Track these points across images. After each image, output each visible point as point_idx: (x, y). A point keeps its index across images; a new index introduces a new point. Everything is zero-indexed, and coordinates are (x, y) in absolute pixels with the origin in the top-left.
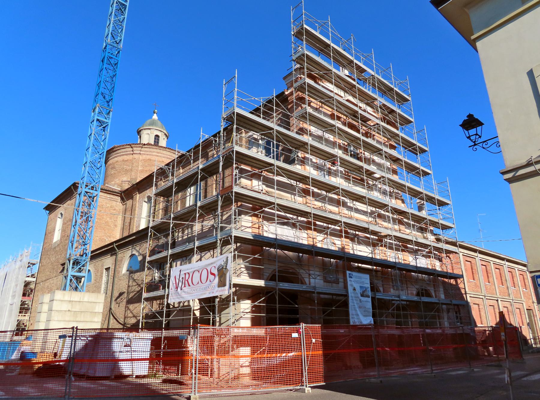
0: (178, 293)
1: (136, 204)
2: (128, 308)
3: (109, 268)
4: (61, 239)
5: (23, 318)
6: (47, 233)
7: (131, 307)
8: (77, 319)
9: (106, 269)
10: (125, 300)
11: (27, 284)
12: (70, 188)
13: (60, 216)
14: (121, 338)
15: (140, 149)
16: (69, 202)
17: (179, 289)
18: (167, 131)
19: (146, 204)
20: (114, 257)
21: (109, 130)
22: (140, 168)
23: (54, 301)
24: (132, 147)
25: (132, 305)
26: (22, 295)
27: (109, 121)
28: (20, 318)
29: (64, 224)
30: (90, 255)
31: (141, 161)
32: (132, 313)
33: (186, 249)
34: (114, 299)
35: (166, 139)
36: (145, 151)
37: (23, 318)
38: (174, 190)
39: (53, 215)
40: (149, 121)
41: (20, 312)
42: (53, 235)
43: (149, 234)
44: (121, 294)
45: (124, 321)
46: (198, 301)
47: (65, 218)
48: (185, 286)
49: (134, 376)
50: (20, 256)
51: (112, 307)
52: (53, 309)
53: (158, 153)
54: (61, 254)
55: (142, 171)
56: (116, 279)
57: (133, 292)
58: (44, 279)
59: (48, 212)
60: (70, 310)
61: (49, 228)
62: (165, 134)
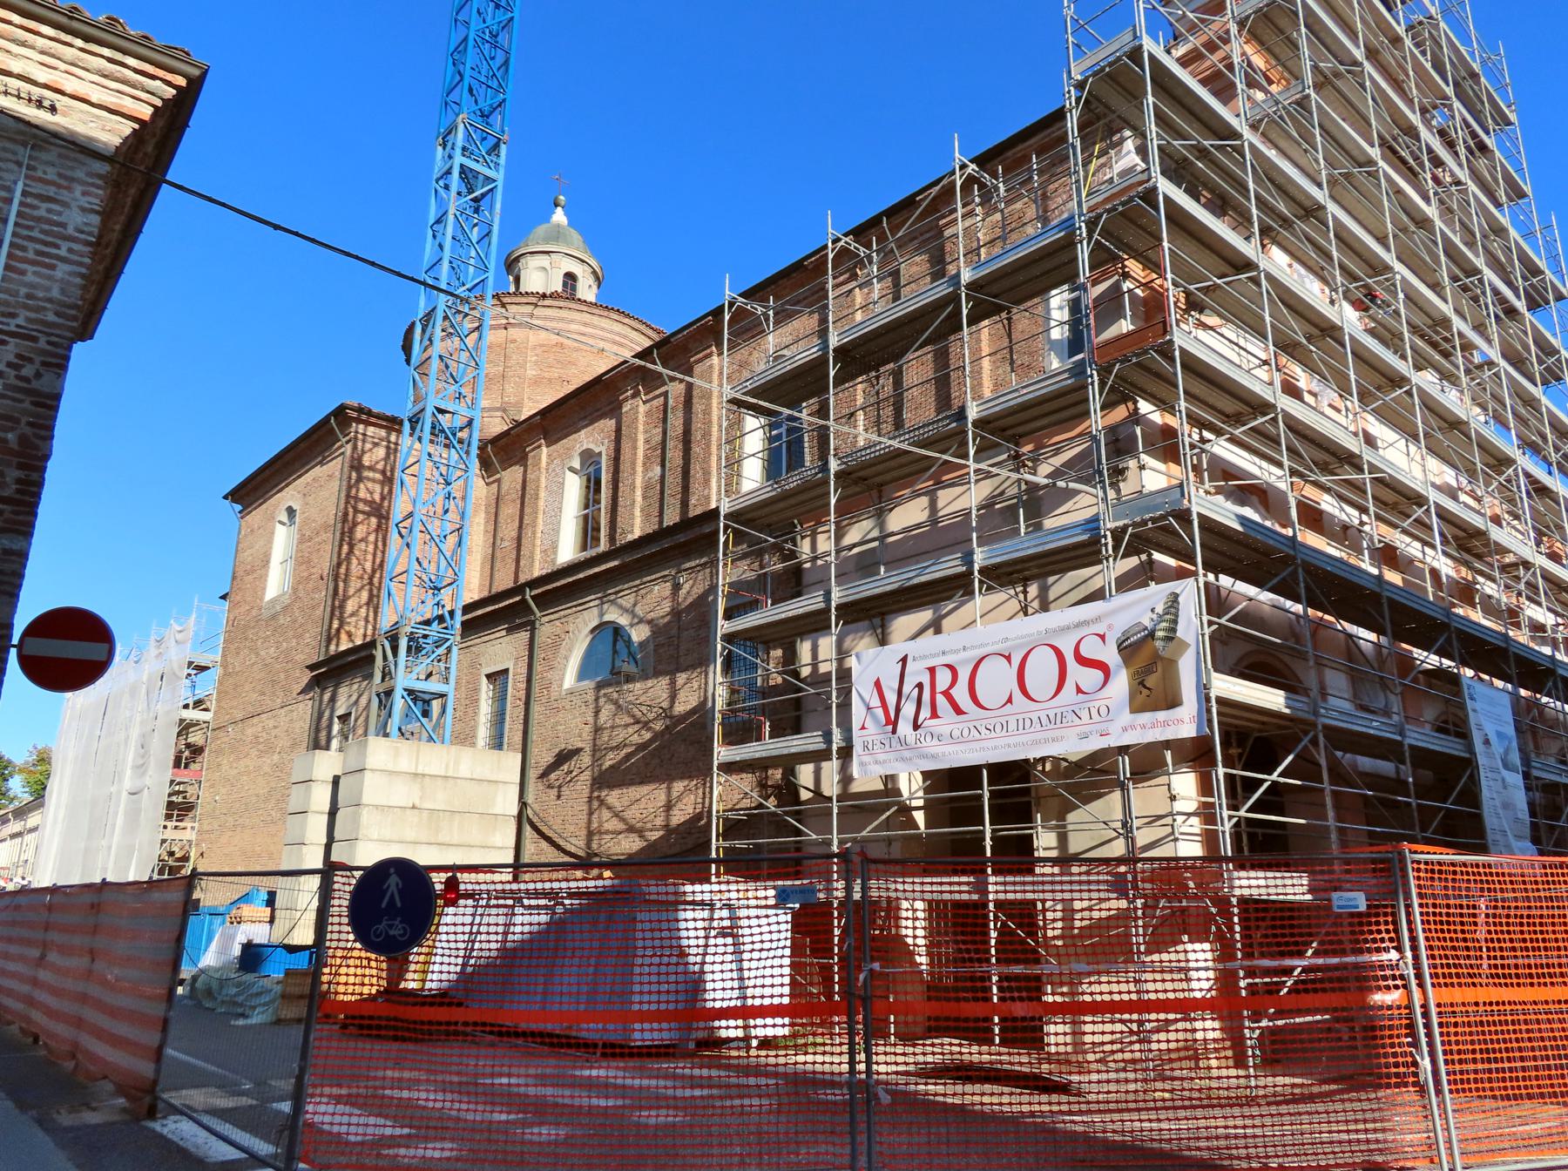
0: (903, 742)
1: (538, 480)
2: (602, 802)
3: (506, 671)
4: (295, 590)
5: (178, 835)
6: (240, 573)
7: (614, 797)
8: (440, 840)
9: (488, 676)
10: (587, 776)
11: (185, 727)
12: (325, 422)
13: (284, 517)
14: (702, 903)
15: (529, 309)
16: (317, 471)
17: (904, 728)
18: (595, 255)
19: (576, 477)
20: (524, 636)
21: (498, 206)
22: (531, 372)
23: (367, 774)
24: (503, 305)
25: (616, 793)
26: (171, 764)
27: (499, 176)
28: (169, 834)
29: (303, 539)
30: (459, 618)
31: (534, 348)
32: (623, 820)
33: (923, 579)
34: (532, 774)
35: (595, 287)
36: (546, 318)
37: (178, 835)
38: (832, 373)
39: (256, 516)
40: (541, 230)
41: (168, 817)
42: (263, 578)
43: (722, 539)
44: (563, 757)
45: (588, 845)
46: (920, 778)
47: (305, 522)
48: (934, 715)
49: (754, 1043)
50: (153, 643)
51: (530, 799)
52: (365, 800)
53: (585, 324)
54: (301, 636)
55: (537, 382)
56: (536, 708)
57: (617, 747)
58: (240, 716)
59: (238, 507)
60: (418, 804)
61: (246, 556)
62: (594, 272)
